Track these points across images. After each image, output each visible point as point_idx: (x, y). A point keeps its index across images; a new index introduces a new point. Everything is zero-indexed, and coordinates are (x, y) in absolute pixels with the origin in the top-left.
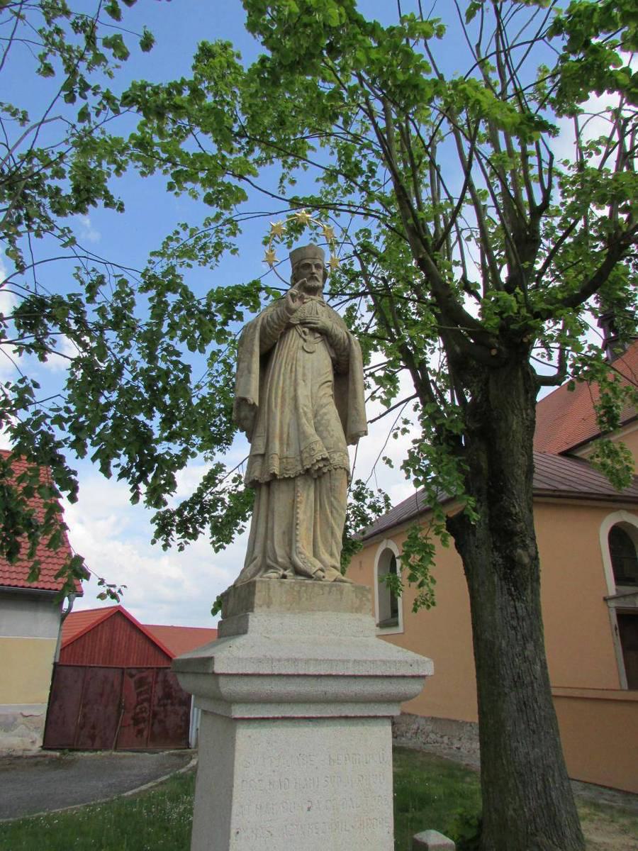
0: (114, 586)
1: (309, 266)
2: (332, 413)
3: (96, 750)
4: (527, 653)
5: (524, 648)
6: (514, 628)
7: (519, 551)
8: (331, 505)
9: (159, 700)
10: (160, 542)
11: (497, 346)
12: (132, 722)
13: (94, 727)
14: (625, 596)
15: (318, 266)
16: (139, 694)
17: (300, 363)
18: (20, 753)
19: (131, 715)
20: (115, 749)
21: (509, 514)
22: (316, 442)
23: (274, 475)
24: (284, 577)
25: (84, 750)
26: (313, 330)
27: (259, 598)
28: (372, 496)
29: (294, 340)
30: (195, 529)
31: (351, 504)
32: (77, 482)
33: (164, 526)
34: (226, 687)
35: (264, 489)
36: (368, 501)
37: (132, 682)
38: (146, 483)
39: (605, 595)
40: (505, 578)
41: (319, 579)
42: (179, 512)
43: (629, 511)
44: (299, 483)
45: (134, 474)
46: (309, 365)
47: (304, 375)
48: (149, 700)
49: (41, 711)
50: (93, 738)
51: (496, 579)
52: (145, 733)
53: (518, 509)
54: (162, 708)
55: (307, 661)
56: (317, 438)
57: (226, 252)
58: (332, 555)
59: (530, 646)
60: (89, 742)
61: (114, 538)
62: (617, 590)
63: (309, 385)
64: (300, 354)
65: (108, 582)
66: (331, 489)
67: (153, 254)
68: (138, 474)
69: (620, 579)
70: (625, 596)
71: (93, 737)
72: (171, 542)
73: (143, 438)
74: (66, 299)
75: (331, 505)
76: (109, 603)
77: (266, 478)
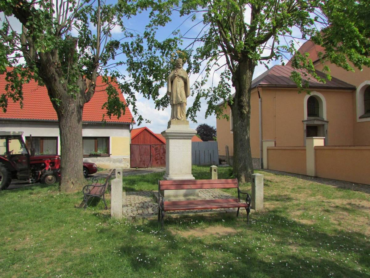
2: (184, 92)
3: (146, 168)
5: (243, 133)
6: (241, 128)
7: (244, 110)
9: (162, 154)
10: (157, 108)
13: (144, 162)
14: (310, 120)
15: (181, 63)
16: (156, 152)
19: (154, 158)
25: (142, 168)
26: (180, 77)
29: (176, 79)
30: (166, 105)
33: (158, 104)
34: (168, 134)
37: (154, 148)
39: (303, 120)
42: (161, 100)
43: (317, 91)
49: (128, 157)
50: (144, 165)
52: (159, 163)
53: (245, 100)
59: (245, 133)
64: (178, 82)
67: (147, 26)
69: (309, 115)
70: (310, 120)
71: (144, 164)
73: (150, 83)
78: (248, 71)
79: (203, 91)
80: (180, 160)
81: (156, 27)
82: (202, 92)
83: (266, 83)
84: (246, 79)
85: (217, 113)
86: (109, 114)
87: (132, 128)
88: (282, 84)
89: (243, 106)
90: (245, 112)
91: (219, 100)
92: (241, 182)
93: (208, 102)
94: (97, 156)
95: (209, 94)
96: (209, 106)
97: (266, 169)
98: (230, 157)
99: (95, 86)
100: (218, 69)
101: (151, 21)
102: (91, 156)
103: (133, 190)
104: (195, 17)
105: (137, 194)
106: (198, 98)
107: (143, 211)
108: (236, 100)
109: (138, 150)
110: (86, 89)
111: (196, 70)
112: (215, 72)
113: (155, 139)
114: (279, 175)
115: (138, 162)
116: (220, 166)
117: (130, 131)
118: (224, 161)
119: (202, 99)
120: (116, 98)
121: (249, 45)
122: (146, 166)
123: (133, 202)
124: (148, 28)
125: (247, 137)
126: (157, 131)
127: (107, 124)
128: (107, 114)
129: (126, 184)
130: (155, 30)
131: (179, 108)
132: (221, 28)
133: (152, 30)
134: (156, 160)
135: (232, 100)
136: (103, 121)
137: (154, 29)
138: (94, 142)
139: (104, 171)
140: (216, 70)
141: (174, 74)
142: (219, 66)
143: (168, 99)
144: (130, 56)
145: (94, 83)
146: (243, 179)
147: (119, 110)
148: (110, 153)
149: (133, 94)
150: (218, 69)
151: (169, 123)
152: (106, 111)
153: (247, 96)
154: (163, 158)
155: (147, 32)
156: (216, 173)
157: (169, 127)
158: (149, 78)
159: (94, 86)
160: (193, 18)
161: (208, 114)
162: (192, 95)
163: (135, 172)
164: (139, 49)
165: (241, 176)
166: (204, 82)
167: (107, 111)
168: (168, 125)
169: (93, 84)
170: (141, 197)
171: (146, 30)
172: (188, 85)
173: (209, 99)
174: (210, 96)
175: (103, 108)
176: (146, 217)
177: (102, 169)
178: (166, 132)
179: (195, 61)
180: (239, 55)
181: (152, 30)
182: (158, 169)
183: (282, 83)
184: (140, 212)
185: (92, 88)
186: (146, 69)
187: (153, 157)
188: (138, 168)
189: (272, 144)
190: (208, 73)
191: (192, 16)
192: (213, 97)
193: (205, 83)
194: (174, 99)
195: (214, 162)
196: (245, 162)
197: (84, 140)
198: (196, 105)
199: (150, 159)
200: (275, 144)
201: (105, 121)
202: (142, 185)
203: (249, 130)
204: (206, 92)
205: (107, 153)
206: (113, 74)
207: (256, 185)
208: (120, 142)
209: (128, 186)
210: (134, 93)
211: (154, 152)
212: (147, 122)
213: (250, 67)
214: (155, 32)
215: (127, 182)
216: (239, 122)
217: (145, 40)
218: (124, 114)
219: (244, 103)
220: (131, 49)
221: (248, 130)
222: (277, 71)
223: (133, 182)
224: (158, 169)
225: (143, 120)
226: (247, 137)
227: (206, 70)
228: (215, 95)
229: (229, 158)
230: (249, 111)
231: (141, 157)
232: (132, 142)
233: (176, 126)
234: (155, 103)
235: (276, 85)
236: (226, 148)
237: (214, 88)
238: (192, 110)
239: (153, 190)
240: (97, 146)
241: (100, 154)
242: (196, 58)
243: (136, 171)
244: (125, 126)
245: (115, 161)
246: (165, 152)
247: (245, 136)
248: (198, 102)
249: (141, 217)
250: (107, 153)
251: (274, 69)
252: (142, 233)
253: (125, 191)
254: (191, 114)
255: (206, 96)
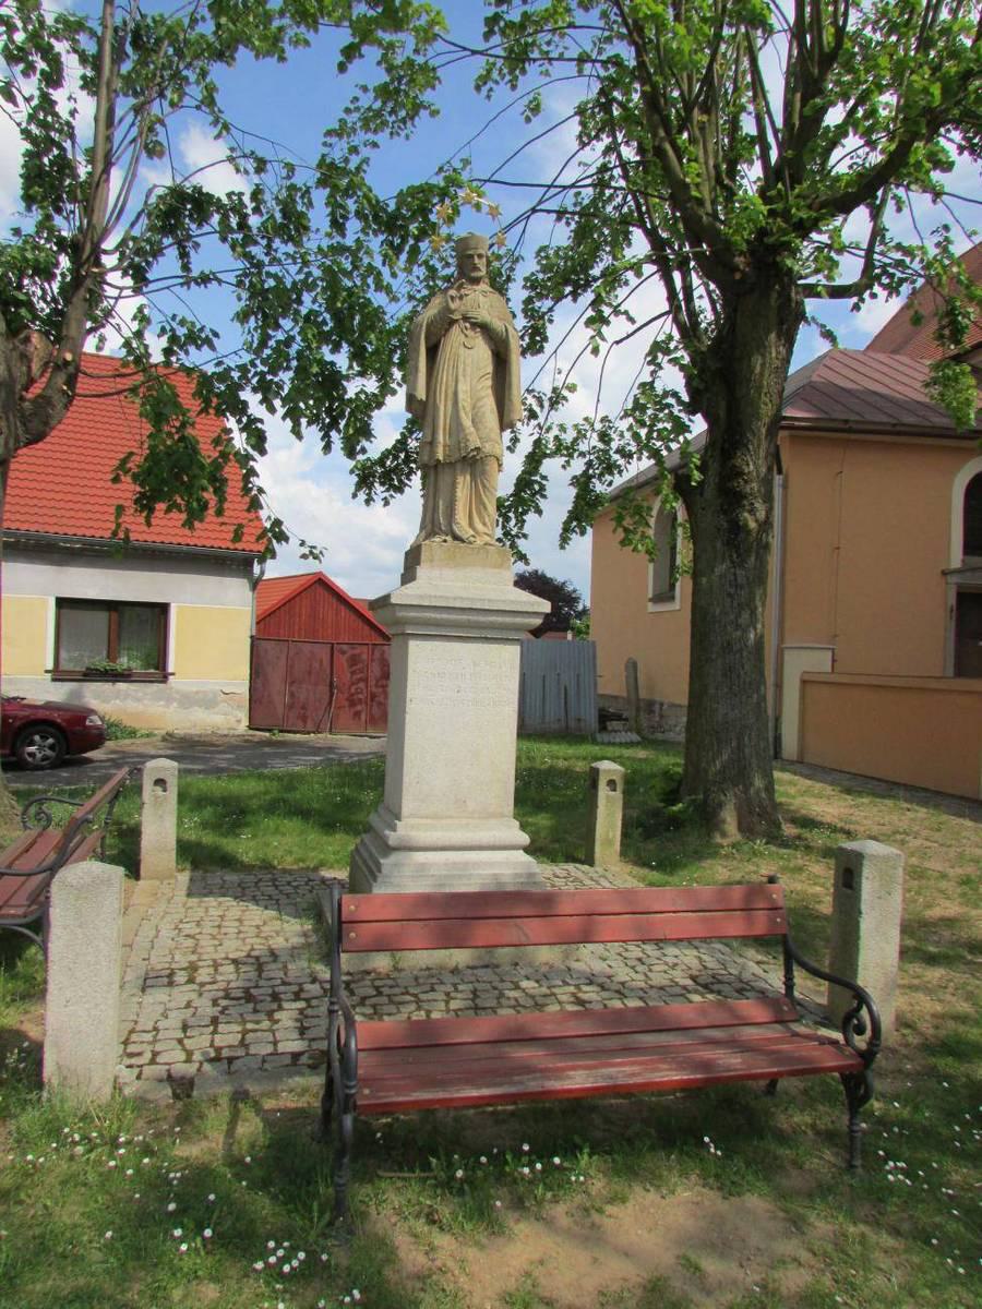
0: (314, 547)
1: (472, 256)
2: (489, 403)
3: (309, 733)
4: (740, 621)
5: (739, 615)
6: (729, 595)
7: (746, 514)
8: (484, 486)
10: (362, 496)
11: (741, 267)
12: (346, 703)
15: (480, 256)
16: (353, 673)
17: (462, 359)
18: (226, 732)
20: (331, 732)
21: (740, 474)
22: (471, 434)
23: (438, 461)
24: (445, 541)
25: (295, 732)
26: (474, 325)
27: (424, 556)
28: (622, 435)
30: (400, 481)
31: (594, 447)
32: (264, 432)
33: (365, 479)
34: (401, 614)
35: (432, 472)
36: (614, 445)
37: (343, 659)
38: (339, 431)
40: (728, 543)
41: (470, 543)
42: (381, 461)
44: (459, 466)
45: (324, 419)
46: (469, 361)
47: (464, 370)
48: (366, 680)
49: (243, 688)
50: (304, 719)
51: (719, 545)
52: (363, 717)
53: (751, 467)
54: (380, 690)
55: (455, 599)
56: (472, 429)
57: (424, 113)
58: (484, 524)
59: (745, 616)
60: (300, 723)
61: (304, 476)
62: (963, 561)
63: (468, 379)
64: (462, 350)
65: (309, 543)
66: (484, 473)
67: (329, 133)
68: (328, 420)
69: (970, 547)
71: (302, 717)
72: (375, 497)
73: (331, 381)
74: (225, 200)
75: (484, 486)
76: (312, 566)
77: (433, 463)
78: (773, 336)
79: (555, 431)
80: (459, 729)
81: (370, 137)
82: (551, 436)
83: (801, 410)
84: (762, 374)
85: (625, 523)
86: (146, 504)
87: (262, 573)
88: (868, 417)
89: (745, 497)
90: (752, 525)
91: (620, 472)
92: (724, 835)
93: (575, 477)
94: (116, 676)
95: (583, 447)
96: (577, 497)
97: (792, 762)
98: (642, 704)
99: (78, 369)
100: (628, 336)
101: (348, 111)
102: (91, 675)
103: (227, 861)
104: (538, 105)
105: (241, 894)
106: (534, 459)
107: (245, 1032)
108: (714, 467)
109: (283, 661)
110: (31, 381)
111: (533, 342)
112: (609, 365)
113: (353, 617)
114: (860, 794)
115: (280, 710)
116: (606, 737)
117: (255, 584)
118: (619, 718)
119: (550, 466)
120: (182, 439)
121: (786, 215)
122: (310, 727)
123: (209, 951)
124: (334, 140)
125: (752, 636)
126: (359, 588)
127: (135, 549)
128: (136, 502)
129: (205, 825)
130: (365, 152)
131: (463, 485)
132: (662, 133)
133: (354, 150)
134: (352, 704)
135: (697, 468)
136: (115, 534)
137: (362, 149)
138: (106, 621)
139: (138, 741)
140: (617, 342)
141: (447, 310)
142: (632, 320)
143: (407, 457)
144: (248, 257)
145: (69, 357)
146: (729, 819)
147: (189, 489)
148: (171, 669)
149: (259, 425)
150: (628, 336)
151: (413, 558)
152: (129, 489)
153: (762, 453)
154: (381, 699)
155: (328, 161)
156: (618, 795)
157: (408, 576)
158: (328, 357)
159: (71, 369)
160: (528, 106)
161: (573, 531)
162: (509, 448)
163: (267, 750)
164: (292, 224)
165: (720, 805)
166: (565, 393)
167: (138, 489)
168: (406, 568)
169: (66, 363)
170: (256, 914)
171: (326, 150)
172: (514, 380)
173: (578, 466)
174: (582, 454)
175: (116, 480)
176: (253, 1088)
177: (132, 733)
178: (393, 601)
179: (529, 301)
180: (740, 261)
181: (354, 150)
182: (356, 744)
183: (872, 416)
184: (228, 1036)
185: (60, 379)
186: (320, 319)
187: (340, 691)
188: (281, 731)
189: (820, 662)
190: (600, 334)
191: (525, 101)
192: (597, 458)
193: (565, 398)
194: (441, 438)
195: (579, 720)
196: (739, 744)
197: (63, 611)
198: (528, 491)
199: (327, 697)
200: (834, 661)
201: (127, 537)
202: (277, 831)
203: (764, 605)
204: (568, 437)
205: (157, 668)
206: (172, 330)
207: (864, 907)
208: (212, 627)
209: (208, 838)
210: (261, 421)
211: (344, 675)
212: (304, 556)
213: (781, 322)
214: (366, 161)
215: (208, 812)
216: (721, 568)
217: (320, 196)
218: (220, 512)
219: (746, 482)
220: (254, 221)
221: (759, 603)
222: (845, 371)
223: (234, 815)
224: (356, 744)
225: (286, 539)
226: (752, 636)
227: (590, 322)
228: (606, 452)
229: (638, 709)
230: (767, 517)
231: (293, 689)
232: (258, 630)
233: (448, 573)
234: (352, 472)
235: (846, 421)
236: (627, 667)
237: (602, 420)
238: (510, 507)
239: (322, 864)
240: (119, 637)
241: (130, 669)
242: (533, 288)
243: (270, 743)
244: (234, 563)
245: (188, 700)
246: (386, 675)
247: (745, 631)
248: (537, 478)
249: (225, 1091)
250: (157, 668)
251: (828, 362)
252: (204, 1263)
253: (188, 866)
254: (504, 527)
255: (566, 450)
